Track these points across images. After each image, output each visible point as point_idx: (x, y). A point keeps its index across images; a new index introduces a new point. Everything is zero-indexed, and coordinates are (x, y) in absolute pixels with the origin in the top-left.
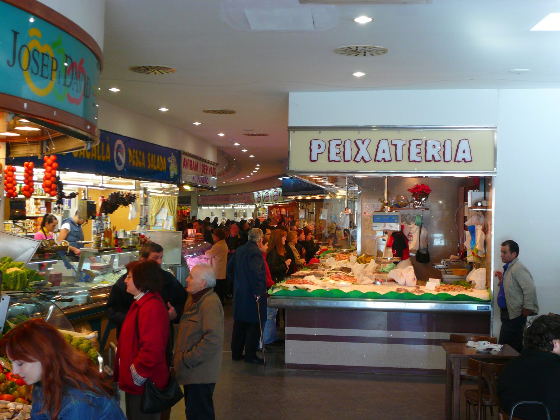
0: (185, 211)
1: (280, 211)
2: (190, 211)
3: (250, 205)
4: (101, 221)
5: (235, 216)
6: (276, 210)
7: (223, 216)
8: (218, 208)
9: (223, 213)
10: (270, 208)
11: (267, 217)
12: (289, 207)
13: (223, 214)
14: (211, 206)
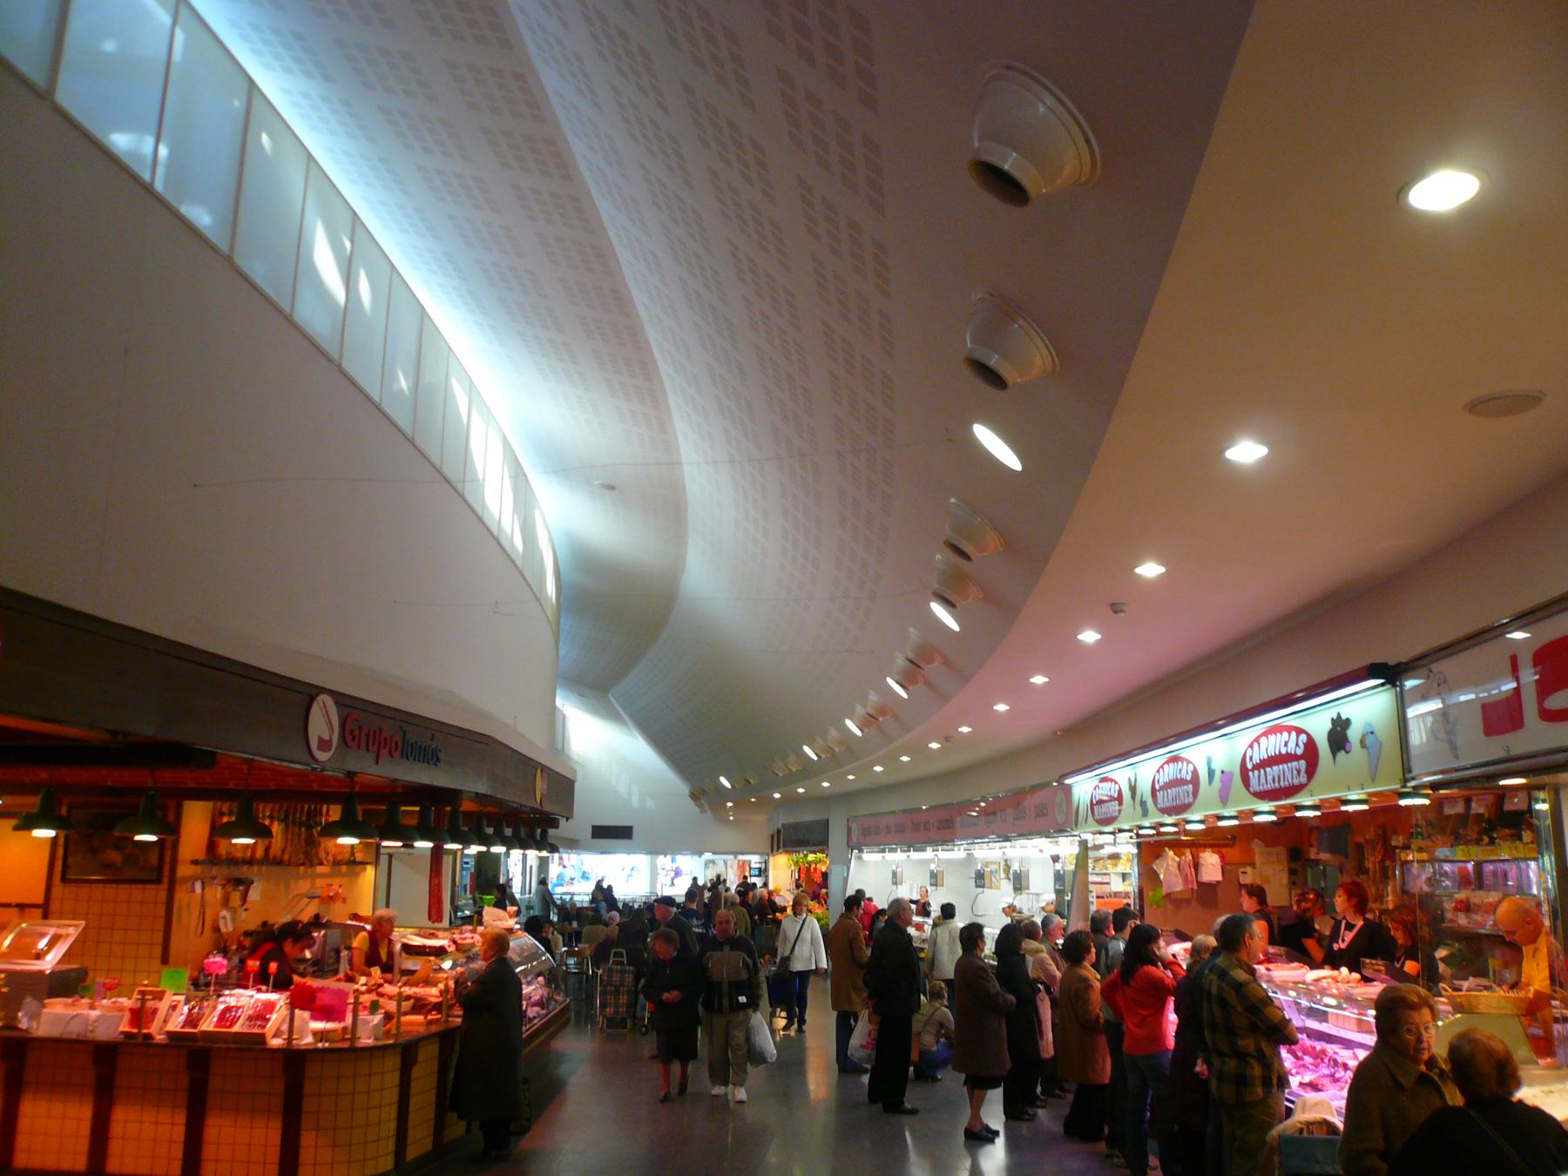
0: (815, 869)
1: (1196, 866)
3: (940, 848)
5: (977, 886)
6: (1178, 859)
8: (915, 855)
10: (1150, 850)
14: (891, 850)
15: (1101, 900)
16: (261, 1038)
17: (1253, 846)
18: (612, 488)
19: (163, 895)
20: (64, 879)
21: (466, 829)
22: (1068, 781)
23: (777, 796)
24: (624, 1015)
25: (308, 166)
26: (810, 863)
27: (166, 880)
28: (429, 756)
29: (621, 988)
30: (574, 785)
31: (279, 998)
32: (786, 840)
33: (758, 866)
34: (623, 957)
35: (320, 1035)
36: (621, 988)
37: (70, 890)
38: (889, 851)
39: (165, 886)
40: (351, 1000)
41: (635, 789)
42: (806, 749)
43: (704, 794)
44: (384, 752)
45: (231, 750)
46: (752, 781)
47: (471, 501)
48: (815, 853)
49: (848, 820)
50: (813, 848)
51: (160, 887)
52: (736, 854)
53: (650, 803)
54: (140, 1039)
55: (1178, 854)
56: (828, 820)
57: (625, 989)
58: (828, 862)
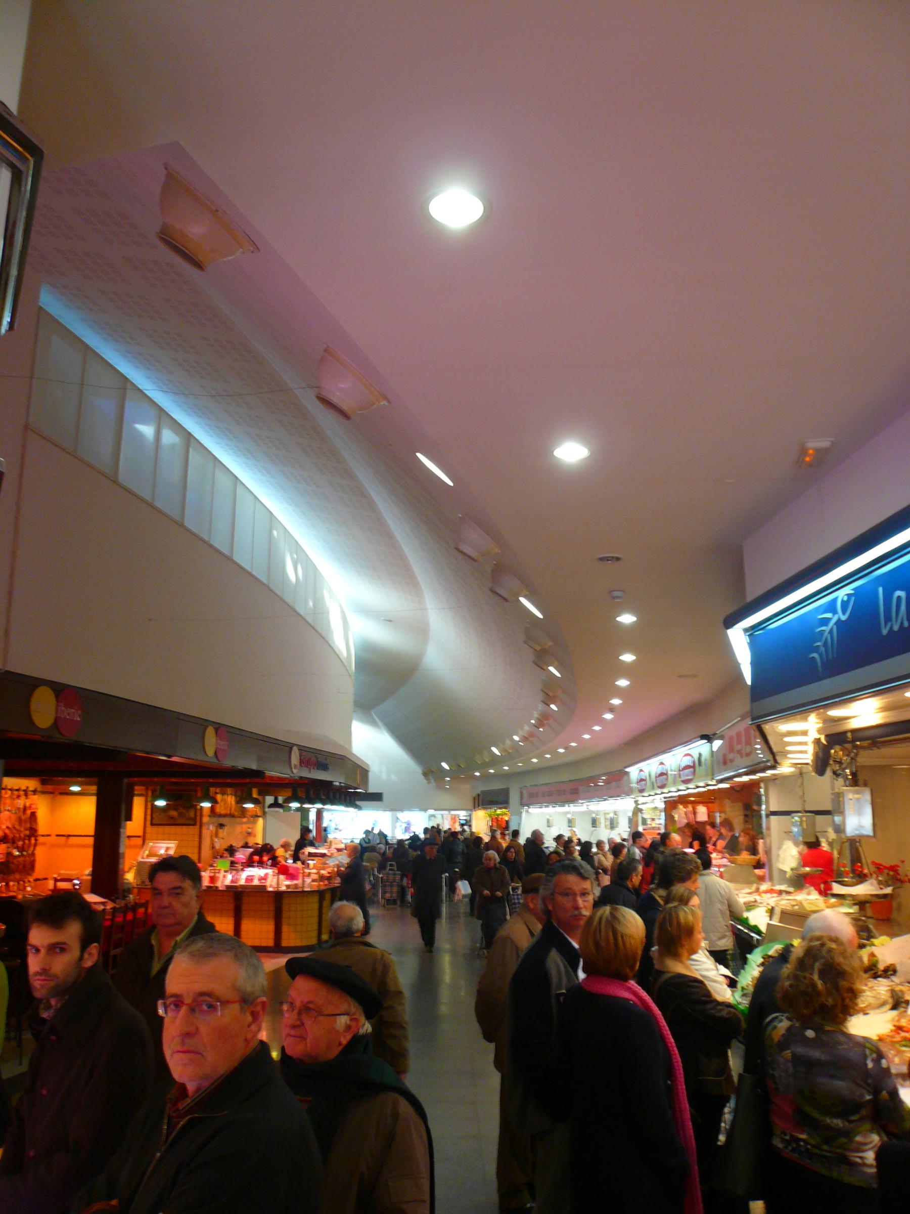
1: (695, 813)
2: (510, 818)
4: (22, 854)
5: (593, 827)
6: (685, 810)
10: (671, 805)
16: (265, 887)
18: (390, 621)
20: (152, 824)
22: (627, 770)
23: (477, 774)
26: (498, 815)
27: (198, 823)
28: (324, 767)
31: (270, 871)
32: (483, 801)
33: (465, 818)
35: (288, 886)
37: (155, 828)
39: (198, 826)
43: (431, 773)
47: (320, 631)
50: (501, 806)
52: (450, 810)
53: (394, 778)
54: (214, 889)
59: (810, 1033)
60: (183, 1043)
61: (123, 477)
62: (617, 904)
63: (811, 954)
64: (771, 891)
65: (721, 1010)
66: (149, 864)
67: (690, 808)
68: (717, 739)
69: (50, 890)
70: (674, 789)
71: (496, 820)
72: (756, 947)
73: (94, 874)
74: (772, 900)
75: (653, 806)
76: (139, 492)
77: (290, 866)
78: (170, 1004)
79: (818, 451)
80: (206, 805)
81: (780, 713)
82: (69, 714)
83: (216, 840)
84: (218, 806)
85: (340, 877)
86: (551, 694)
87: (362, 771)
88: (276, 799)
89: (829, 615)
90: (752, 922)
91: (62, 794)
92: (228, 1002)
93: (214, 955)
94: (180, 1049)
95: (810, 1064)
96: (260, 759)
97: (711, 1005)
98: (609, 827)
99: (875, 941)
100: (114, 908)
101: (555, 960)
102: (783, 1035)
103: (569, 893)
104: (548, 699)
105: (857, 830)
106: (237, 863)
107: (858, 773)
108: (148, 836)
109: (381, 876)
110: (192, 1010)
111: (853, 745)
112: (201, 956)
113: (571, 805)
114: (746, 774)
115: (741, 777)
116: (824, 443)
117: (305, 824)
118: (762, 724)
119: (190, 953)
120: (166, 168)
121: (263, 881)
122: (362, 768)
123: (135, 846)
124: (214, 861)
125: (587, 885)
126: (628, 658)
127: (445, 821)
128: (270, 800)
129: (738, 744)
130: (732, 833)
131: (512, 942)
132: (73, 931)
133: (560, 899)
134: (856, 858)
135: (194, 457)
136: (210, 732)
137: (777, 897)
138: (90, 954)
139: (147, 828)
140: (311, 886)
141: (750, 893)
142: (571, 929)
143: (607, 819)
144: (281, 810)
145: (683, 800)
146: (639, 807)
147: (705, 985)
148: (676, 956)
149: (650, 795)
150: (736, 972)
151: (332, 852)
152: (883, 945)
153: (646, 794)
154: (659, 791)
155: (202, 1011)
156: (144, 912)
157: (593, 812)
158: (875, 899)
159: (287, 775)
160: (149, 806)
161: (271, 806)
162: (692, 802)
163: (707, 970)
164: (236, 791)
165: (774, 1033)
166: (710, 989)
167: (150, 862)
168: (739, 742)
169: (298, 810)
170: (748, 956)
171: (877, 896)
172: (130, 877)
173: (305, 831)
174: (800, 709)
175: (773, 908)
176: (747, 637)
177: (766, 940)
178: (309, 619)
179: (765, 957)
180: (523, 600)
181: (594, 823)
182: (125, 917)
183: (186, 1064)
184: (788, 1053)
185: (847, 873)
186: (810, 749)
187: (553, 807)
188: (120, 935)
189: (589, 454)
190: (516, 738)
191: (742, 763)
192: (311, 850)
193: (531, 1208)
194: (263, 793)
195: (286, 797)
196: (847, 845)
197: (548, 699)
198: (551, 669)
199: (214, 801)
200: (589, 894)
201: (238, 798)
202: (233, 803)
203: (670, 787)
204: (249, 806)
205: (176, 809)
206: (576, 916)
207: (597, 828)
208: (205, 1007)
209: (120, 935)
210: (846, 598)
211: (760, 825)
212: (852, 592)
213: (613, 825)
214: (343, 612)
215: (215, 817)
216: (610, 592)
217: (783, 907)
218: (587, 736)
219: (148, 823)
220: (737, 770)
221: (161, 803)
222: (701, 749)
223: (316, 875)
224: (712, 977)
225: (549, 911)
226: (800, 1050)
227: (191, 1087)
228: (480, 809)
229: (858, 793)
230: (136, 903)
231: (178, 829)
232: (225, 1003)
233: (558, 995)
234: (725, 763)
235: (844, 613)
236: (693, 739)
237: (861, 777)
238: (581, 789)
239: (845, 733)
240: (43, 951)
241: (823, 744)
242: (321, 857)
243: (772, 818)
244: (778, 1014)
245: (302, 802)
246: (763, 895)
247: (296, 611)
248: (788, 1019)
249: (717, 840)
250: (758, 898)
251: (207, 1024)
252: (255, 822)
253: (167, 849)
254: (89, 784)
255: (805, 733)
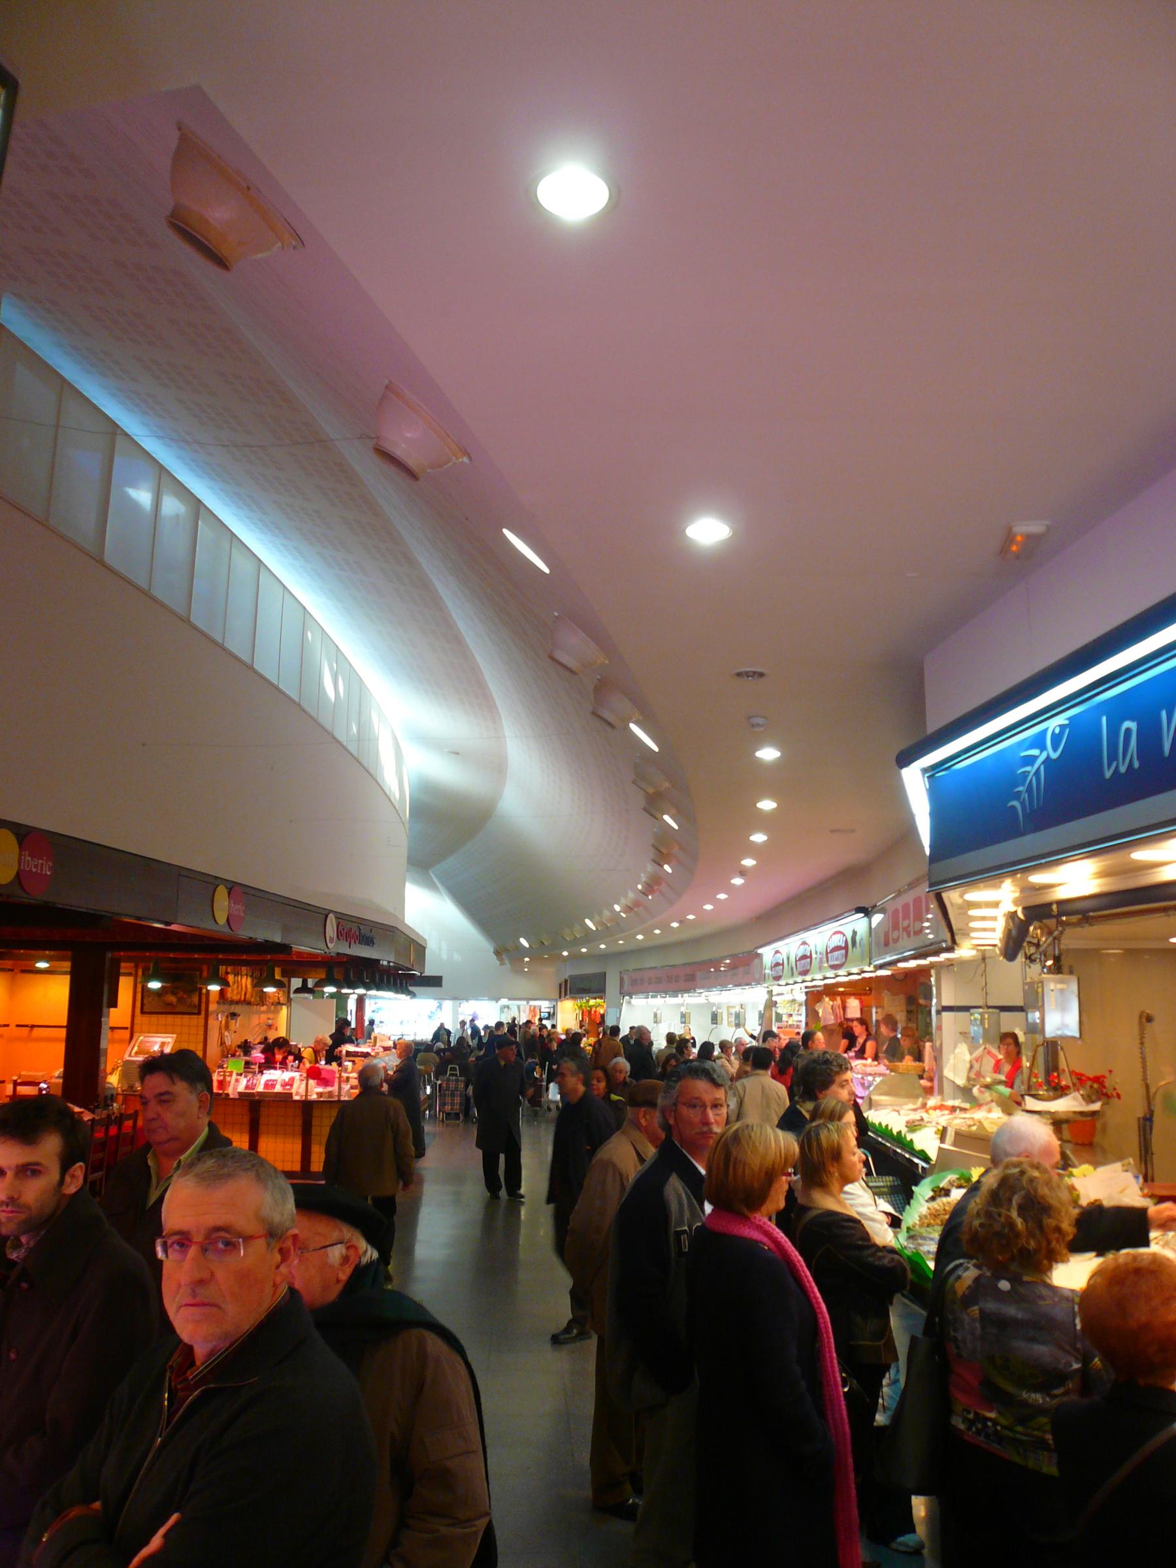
0: (595, 1012)
1: (844, 1008)
5: (712, 1023)
6: (831, 1003)
7: (682, 1023)
9: (683, 1016)
10: (814, 997)
11: (803, 1024)
12: (870, 994)
13: (682, 1017)
15: (781, 1030)
17: (883, 994)
18: (458, 753)
19: (202, 1022)
20: (142, 1012)
21: (368, 981)
22: (760, 951)
23: (565, 953)
24: (458, 1111)
25: (304, 614)
26: (591, 1007)
27: (203, 1013)
28: (368, 941)
29: (456, 1092)
30: (425, 951)
31: (297, 1075)
32: (571, 988)
33: (547, 1010)
34: (456, 1070)
35: (320, 1095)
36: (456, 1092)
37: (146, 1018)
38: (651, 997)
40: (337, 1075)
41: (444, 946)
42: (588, 922)
43: (505, 951)
44: (353, 941)
45: (300, 945)
46: (545, 943)
47: (365, 764)
48: (595, 998)
49: (621, 973)
50: (595, 995)
51: (200, 1016)
52: (528, 999)
53: (456, 957)
54: (223, 1096)
55: (833, 1000)
56: (605, 973)
57: (459, 1093)
58: (605, 1006)
59: (1004, 1285)
60: (194, 1294)
61: (111, 558)
62: (819, 1110)
63: (1007, 1185)
64: (941, 1107)
65: (883, 1257)
66: (138, 1063)
67: (839, 1000)
68: (876, 913)
69: (7, 1096)
70: (819, 976)
71: (587, 1013)
72: (923, 1178)
73: (66, 1076)
74: (943, 1119)
75: (790, 997)
76: (132, 577)
77: (322, 1069)
78: (172, 1244)
79: (1029, 537)
80: (214, 988)
81: (956, 881)
82: (36, 866)
83: (226, 1033)
84: (229, 989)
85: (387, 1083)
86: (664, 851)
87: (418, 948)
88: (305, 982)
89: (1035, 752)
90: (918, 1146)
91: (24, 971)
92: (252, 1237)
93: (229, 1176)
94: (190, 1300)
95: (1003, 1324)
96: (286, 929)
97: (870, 1252)
98: (733, 1024)
99: (1075, 1171)
100: (93, 1120)
101: (675, 1188)
102: (969, 1287)
103: (697, 1104)
104: (661, 857)
105: (1058, 1029)
106: (252, 1064)
107: (1063, 958)
108: (136, 1028)
109: (439, 1082)
110: (204, 1250)
111: (1057, 921)
112: (215, 1178)
113: (686, 995)
114: (914, 957)
115: (908, 962)
116: (1036, 528)
117: (341, 1016)
118: (943, 891)
119: (197, 1175)
120: (179, 129)
121: (288, 1087)
122: (417, 943)
123: (121, 1041)
124: (223, 1061)
125: (720, 1094)
126: (767, 805)
127: (519, 1011)
128: (296, 983)
129: (904, 919)
130: (894, 1034)
131: (614, 1166)
132: (50, 1146)
133: (685, 1111)
134: (1052, 1067)
135: (204, 530)
136: (221, 893)
137: (949, 1114)
138: (73, 1176)
139: (135, 1018)
140: (350, 1095)
141: (915, 1110)
142: (696, 1149)
143: (732, 1014)
144: (311, 997)
145: (830, 991)
146: (774, 999)
147: (863, 1225)
148: (823, 1186)
149: (787, 984)
150: (901, 1210)
151: (376, 1051)
152: (1085, 1176)
153: (782, 982)
154: (799, 979)
155: (217, 1251)
156: (131, 1125)
157: (713, 1004)
158: (1079, 1118)
159: (320, 950)
160: (139, 989)
161: (297, 991)
162: (842, 994)
163: (863, 1205)
164: (252, 971)
165: (957, 1284)
166: (868, 1229)
167: (137, 1061)
168: (906, 916)
169: (332, 996)
170: (914, 1188)
171: (1082, 1113)
172: (113, 1080)
173: (342, 1024)
174: (991, 873)
175: (945, 1129)
176: (926, 779)
177: (936, 1170)
178: (352, 748)
179: (935, 1189)
180: (633, 727)
181: (715, 1018)
182: (107, 1132)
183: (198, 1321)
184: (975, 1310)
185: (1040, 1085)
186: (1000, 926)
187: (661, 997)
188: (100, 1155)
189: (731, 534)
190: (617, 908)
191: (908, 945)
192: (350, 1048)
193: (635, 1505)
194: (289, 974)
195: (318, 980)
196: (1041, 1050)
197: (661, 857)
198: (666, 818)
199: (224, 983)
200: (721, 1106)
201: (255, 981)
202: (249, 986)
203: (813, 974)
204: (270, 990)
205: (173, 993)
206: (705, 1133)
207: (718, 1026)
208: (221, 1246)
209: (100, 1155)
210: (1057, 731)
211: (929, 1024)
212: (1067, 722)
213: (739, 1023)
214: (395, 739)
215: (224, 1004)
216: (749, 718)
217: (958, 1127)
218: (708, 907)
219: (138, 1011)
220: (903, 953)
221: (155, 985)
222: (857, 924)
223: (355, 1080)
224: (868, 1214)
225: (670, 1126)
226: (991, 1306)
227: (200, 1351)
228: (567, 999)
229: (1061, 982)
230: (121, 1114)
231: (178, 1019)
232: (248, 1239)
233: (678, 1234)
234: (886, 944)
235: (1055, 749)
236: (846, 912)
237: (1065, 962)
238: (699, 974)
239: (1050, 904)
240: (10, 1174)
241: (1019, 918)
242: (362, 1057)
243: (945, 1014)
244: (961, 1261)
245: (339, 986)
246: (931, 1112)
247: (334, 737)
248: (977, 1266)
249: (865, 1041)
250: (925, 1116)
251: (224, 1269)
252: (277, 1012)
253: (163, 1044)
254: (63, 959)
255: (996, 905)
